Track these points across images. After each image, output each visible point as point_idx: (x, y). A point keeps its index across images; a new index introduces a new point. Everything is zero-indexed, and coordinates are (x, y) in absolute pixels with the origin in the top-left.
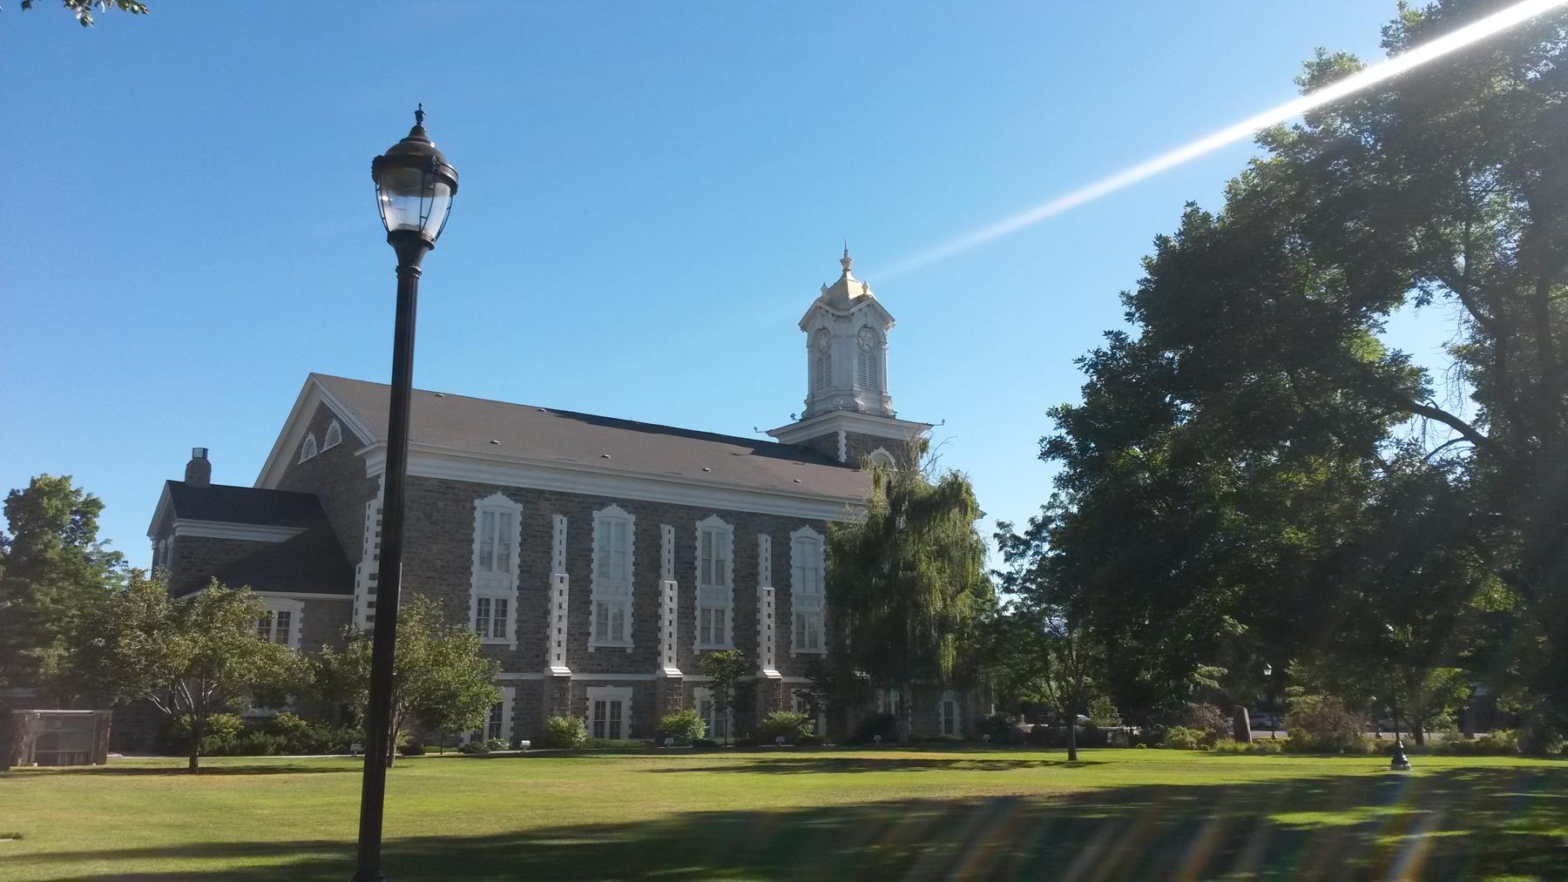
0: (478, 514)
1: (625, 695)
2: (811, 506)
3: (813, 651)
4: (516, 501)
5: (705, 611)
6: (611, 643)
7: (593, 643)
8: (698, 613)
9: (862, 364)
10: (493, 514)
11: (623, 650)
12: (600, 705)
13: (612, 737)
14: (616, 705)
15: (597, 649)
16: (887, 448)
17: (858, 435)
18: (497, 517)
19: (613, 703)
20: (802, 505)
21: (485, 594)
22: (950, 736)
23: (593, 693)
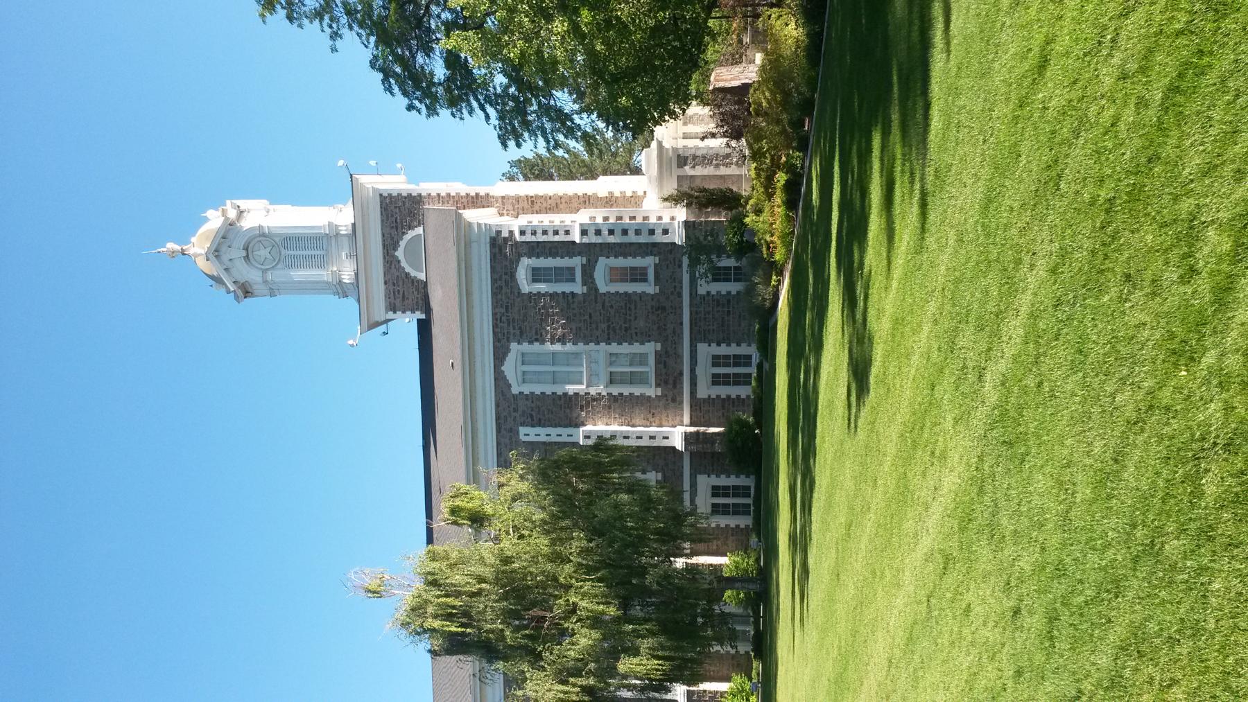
0: (526, 389)
1: (705, 482)
2: (480, 417)
3: (652, 360)
4: (508, 350)
5: (613, 379)
6: (650, 369)
7: (652, 391)
8: (615, 391)
9: (295, 263)
10: (524, 373)
11: (656, 265)
12: (717, 380)
13: (749, 364)
14: (717, 491)
15: (658, 385)
16: (395, 247)
17: (387, 296)
18: (525, 368)
19: (714, 495)
20: (481, 435)
21: (604, 377)
22: (755, 360)
23: (702, 393)
